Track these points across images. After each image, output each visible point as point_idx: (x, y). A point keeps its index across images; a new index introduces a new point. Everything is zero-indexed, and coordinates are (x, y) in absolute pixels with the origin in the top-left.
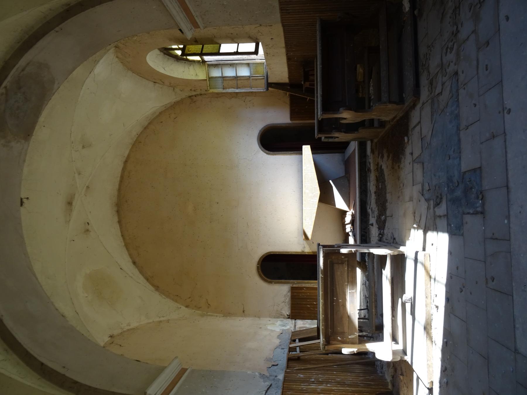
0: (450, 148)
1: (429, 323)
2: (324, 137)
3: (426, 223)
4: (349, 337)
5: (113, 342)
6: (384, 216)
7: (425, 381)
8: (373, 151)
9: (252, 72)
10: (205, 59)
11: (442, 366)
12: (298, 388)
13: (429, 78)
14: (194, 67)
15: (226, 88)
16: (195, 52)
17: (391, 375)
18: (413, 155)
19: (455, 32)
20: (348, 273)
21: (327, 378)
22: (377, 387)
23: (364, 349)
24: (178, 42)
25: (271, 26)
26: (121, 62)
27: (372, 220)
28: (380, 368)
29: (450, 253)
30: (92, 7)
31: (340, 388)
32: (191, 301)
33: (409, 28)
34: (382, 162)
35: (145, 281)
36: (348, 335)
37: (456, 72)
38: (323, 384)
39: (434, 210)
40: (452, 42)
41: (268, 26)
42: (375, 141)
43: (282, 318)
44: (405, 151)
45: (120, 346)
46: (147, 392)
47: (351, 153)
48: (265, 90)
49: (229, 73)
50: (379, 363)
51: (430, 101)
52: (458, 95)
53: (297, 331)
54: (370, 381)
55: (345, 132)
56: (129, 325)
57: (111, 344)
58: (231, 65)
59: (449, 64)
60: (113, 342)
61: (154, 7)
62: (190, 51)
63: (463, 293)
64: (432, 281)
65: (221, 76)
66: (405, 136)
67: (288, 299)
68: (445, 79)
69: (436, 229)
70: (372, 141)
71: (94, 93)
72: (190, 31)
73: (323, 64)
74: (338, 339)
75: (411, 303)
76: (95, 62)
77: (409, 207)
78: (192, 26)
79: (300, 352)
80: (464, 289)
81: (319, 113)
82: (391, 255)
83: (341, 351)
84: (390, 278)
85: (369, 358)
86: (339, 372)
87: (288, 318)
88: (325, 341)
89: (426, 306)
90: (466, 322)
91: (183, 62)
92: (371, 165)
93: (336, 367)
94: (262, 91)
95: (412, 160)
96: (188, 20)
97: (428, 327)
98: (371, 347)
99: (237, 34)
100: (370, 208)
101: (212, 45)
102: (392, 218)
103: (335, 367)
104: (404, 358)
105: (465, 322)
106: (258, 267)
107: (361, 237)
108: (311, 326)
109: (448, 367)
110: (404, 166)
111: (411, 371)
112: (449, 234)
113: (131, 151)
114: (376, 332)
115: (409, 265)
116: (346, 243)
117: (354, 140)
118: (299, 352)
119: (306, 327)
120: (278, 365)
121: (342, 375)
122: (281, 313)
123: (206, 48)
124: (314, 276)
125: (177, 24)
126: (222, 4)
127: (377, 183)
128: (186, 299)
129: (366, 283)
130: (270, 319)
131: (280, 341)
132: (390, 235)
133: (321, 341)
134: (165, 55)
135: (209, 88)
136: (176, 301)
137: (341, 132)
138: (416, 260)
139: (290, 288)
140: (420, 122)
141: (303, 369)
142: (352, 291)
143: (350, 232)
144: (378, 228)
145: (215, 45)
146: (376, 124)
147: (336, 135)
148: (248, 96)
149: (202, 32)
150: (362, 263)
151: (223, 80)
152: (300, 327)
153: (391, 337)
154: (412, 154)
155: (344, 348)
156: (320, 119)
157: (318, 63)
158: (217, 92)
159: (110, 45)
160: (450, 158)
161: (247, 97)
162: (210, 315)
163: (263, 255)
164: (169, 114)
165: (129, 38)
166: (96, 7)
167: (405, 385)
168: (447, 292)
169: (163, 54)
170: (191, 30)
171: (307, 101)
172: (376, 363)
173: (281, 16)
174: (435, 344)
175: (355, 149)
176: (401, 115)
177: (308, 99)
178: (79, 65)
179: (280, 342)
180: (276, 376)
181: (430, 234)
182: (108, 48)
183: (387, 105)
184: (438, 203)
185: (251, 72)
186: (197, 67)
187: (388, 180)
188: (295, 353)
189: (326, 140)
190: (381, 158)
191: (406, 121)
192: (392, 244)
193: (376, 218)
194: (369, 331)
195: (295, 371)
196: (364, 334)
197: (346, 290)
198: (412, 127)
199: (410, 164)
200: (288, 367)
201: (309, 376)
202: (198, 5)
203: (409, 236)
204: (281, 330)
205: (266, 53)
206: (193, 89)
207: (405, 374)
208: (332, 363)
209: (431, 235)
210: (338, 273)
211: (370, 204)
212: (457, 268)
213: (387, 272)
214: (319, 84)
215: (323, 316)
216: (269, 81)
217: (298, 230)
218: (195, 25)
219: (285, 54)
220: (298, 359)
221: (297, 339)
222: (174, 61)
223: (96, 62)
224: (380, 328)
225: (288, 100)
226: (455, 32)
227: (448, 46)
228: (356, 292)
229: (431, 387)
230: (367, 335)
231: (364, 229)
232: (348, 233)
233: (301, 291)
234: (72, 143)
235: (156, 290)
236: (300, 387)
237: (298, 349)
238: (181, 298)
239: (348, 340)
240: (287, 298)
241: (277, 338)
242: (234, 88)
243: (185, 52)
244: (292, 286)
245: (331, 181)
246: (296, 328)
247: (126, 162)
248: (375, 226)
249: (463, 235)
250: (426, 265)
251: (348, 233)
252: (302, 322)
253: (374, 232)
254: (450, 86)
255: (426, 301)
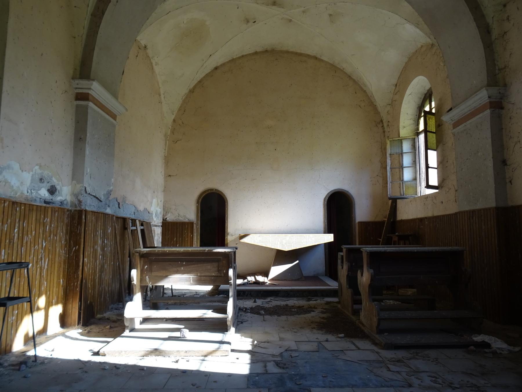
0: (334, 378)
1: (161, 354)
2: (343, 254)
3: (258, 353)
4: (147, 277)
5: (140, 49)
6: (264, 313)
7: (106, 349)
8: (328, 303)
9: (407, 183)
10: (420, 135)
11: (120, 365)
12: (99, 227)
13: (404, 359)
14: (412, 124)
15: (390, 157)
16: (428, 125)
17: (109, 317)
18: (326, 342)
19: (453, 385)
20: (210, 276)
21: (107, 256)
22: (99, 302)
23: (136, 291)
24: (438, 108)
25: (456, 201)
26: (416, 51)
27: (259, 302)
28: (116, 307)
29: (230, 375)
30: (474, 19)
31: (98, 268)
32: (179, 125)
33: (456, 340)
34: (318, 313)
35: (199, 79)
36: (149, 276)
37: (411, 386)
38: (102, 251)
39: (272, 361)
40: (442, 382)
41: (455, 199)
42: (339, 306)
43: (164, 213)
44: (329, 334)
45: (137, 56)
46: (94, 81)
47: (326, 282)
48: (389, 196)
49: (407, 160)
50: (121, 306)
51: (381, 359)
52: (388, 387)
53: (151, 228)
54: (104, 297)
55: (347, 276)
56: (157, 64)
57: (139, 46)
58: (414, 161)
59: (419, 379)
60: (140, 49)
61: (475, 82)
62: (429, 120)
63: (191, 386)
64: (202, 358)
65: (404, 152)
66: (345, 335)
67: (181, 219)
68: (404, 374)
69: (253, 362)
70: (339, 303)
71: (385, 24)
72: (450, 119)
73: (418, 252)
74: (145, 266)
75: (180, 337)
76: (417, 24)
77: (274, 337)
78: (455, 121)
79: (132, 230)
80: (195, 387)
81: (367, 249)
82: (226, 318)
83: (134, 269)
84: (204, 317)
85: (126, 297)
86: (113, 268)
87: (163, 219)
88: (144, 253)
89: (178, 351)
90: (163, 388)
91: (417, 113)
92: (315, 302)
93: (117, 265)
94: (389, 193)
95: (321, 341)
96: (461, 117)
97: (157, 353)
98: (138, 297)
99: (447, 167)
100: (271, 300)
101: (435, 141)
102: (263, 321)
103: (117, 263)
104: (127, 329)
105: (164, 387)
106: (212, 190)
107: (242, 291)
108: (156, 241)
109: (120, 371)
110: (314, 333)
111: (115, 336)
112: (249, 374)
113: (327, 63)
114: (152, 303)
115: (217, 336)
116: (237, 276)
117: (340, 285)
118: (131, 229)
119: (155, 237)
120: (119, 209)
121: (110, 270)
122: (169, 212)
123: (432, 136)
124: (203, 244)
125: (457, 106)
126: (478, 151)
127: (297, 307)
128: (181, 119)
129: (198, 295)
130: (162, 201)
131: (142, 211)
132: (246, 318)
133: (142, 249)
134: (424, 95)
135: (391, 139)
136: (179, 110)
137: (348, 271)
138: (222, 342)
139: (192, 221)
140: (359, 349)
141: (115, 232)
142: (192, 280)
143: (247, 281)
144: (252, 307)
145: (435, 145)
146: (356, 307)
147: (345, 267)
148: (383, 179)
149: (449, 131)
150: (217, 291)
151: (399, 154)
152: (154, 231)
153: (147, 317)
154: (327, 341)
155: (137, 271)
156: (361, 250)
157: (418, 248)
158: (387, 148)
159: (435, 38)
160: (324, 377)
161: (382, 178)
162: (166, 143)
163: (225, 196)
164: (364, 101)
165: (442, 58)
166: (475, 23)
167: (100, 330)
168: (192, 371)
169: (425, 93)
170: (451, 120)
171: (378, 239)
172: (121, 303)
173: (467, 211)
174: (141, 359)
175: (330, 286)
176: (366, 331)
177: (380, 240)
178: (413, 8)
179: (140, 211)
180: (109, 206)
181: (248, 356)
182: (432, 37)
183: (376, 317)
184: (279, 365)
185: (407, 181)
186: (413, 127)
187: (300, 317)
188: (131, 225)
189: (339, 257)
190: (322, 311)
191: (360, 335)
192: (237, 320)
193: (262, 305)
194: (152, 296)
195: (114, 225)
196: (149, 293)
197: (193, 274)
198: (354, 342)
199: (317, 338)
200: (117, 218)
201: (109, 239)
202: (477, 126)
203: (246, 337)
204: (152, 212)
205: (427, 197)
206: (389, 124)
207: (112, 330)
208: (121, 261)
209: (247, 357)
210: (209, 266)
211: (275, 300)
212: (215, 382)
213: (210, 314)
214: (397, 248)
215: (168, 251)
216: (398, 200)
217: (249, 229)
218: (456, 124)
219: (426, 216)
220: (125, 228)
221: (144, 227)
222: (419, 105)
223: (417, 25)
224: (155, 307)
225: (379, 219)
226: (453, 385)
227: (438, 378)
228: (191, 284)
229: (100, 354)
230: (148, 296)
231: (250, 294)
232: (246, 278)
233: (189, 231)
234: (335, 4)
235: (189, 90)
236: (99, 229)
237: (134, 228)
238: (182, 115)
239: (144, 275)
240: (182, 218)
241: (145, 208)
242: (391, 165)
243: (428, 115)
244: (194, 223)
245: (297, 261)
246: (154, 226)
247: (316, 58)
248: (254, 305)
249: (248, 388)
250: (217, 352)
251: (246, 278)
252: (160, 233)
253: (248, 303)
254: (396, 379)
255: (182, 351)
